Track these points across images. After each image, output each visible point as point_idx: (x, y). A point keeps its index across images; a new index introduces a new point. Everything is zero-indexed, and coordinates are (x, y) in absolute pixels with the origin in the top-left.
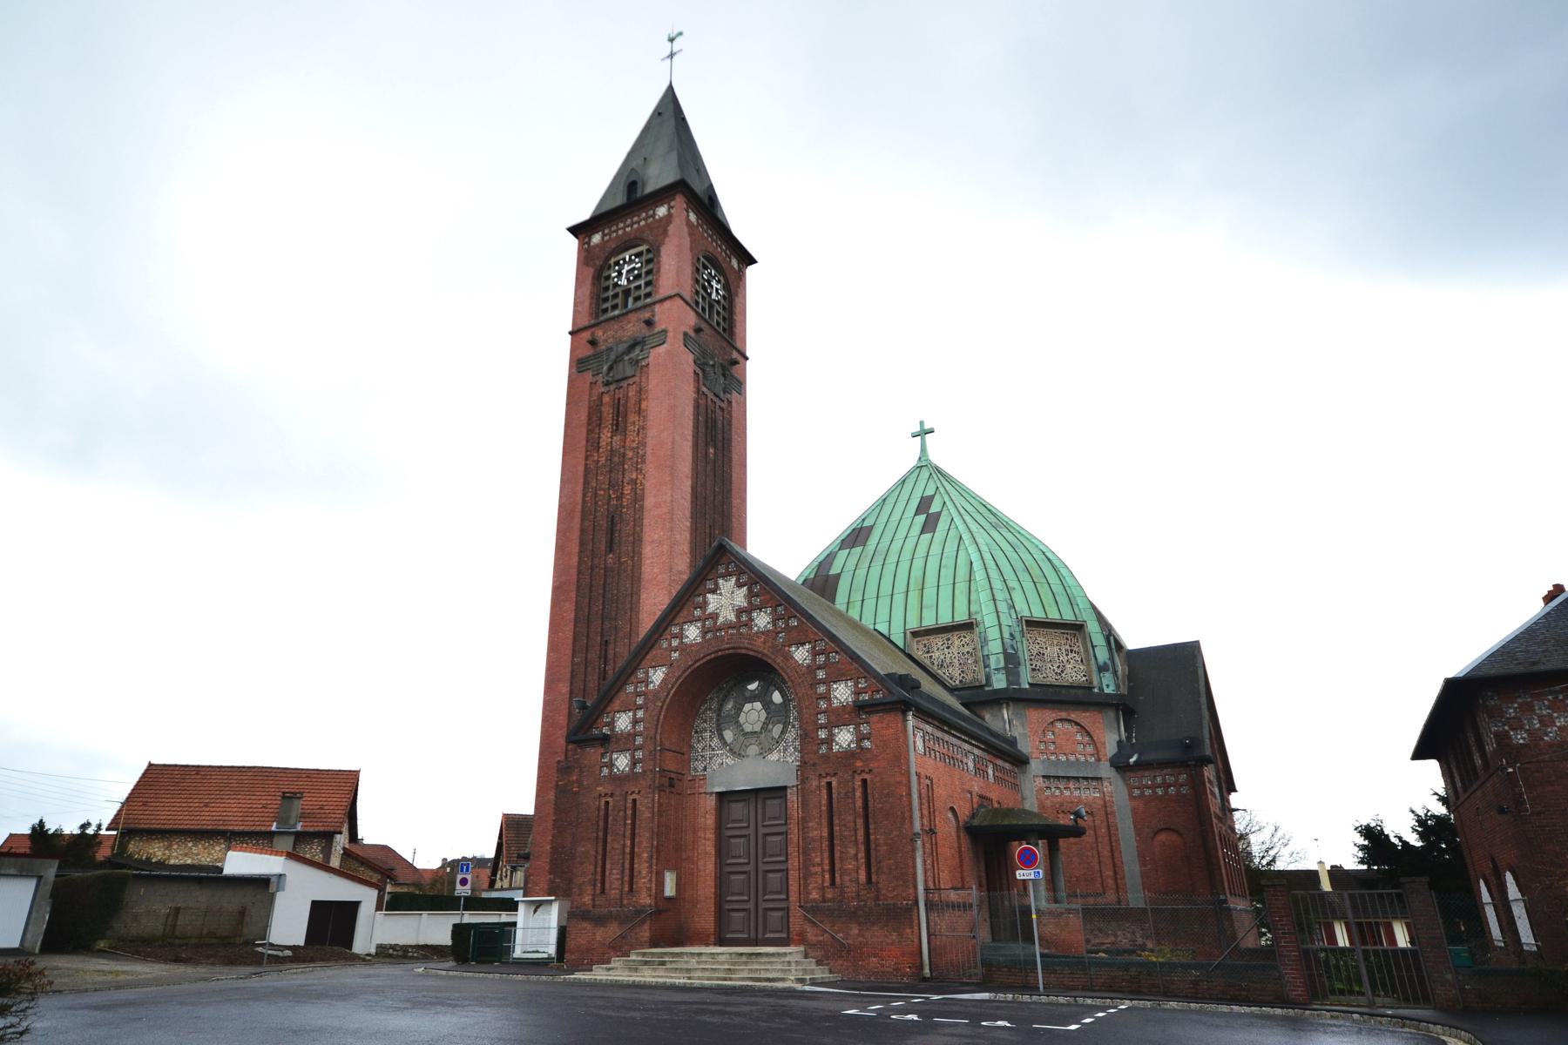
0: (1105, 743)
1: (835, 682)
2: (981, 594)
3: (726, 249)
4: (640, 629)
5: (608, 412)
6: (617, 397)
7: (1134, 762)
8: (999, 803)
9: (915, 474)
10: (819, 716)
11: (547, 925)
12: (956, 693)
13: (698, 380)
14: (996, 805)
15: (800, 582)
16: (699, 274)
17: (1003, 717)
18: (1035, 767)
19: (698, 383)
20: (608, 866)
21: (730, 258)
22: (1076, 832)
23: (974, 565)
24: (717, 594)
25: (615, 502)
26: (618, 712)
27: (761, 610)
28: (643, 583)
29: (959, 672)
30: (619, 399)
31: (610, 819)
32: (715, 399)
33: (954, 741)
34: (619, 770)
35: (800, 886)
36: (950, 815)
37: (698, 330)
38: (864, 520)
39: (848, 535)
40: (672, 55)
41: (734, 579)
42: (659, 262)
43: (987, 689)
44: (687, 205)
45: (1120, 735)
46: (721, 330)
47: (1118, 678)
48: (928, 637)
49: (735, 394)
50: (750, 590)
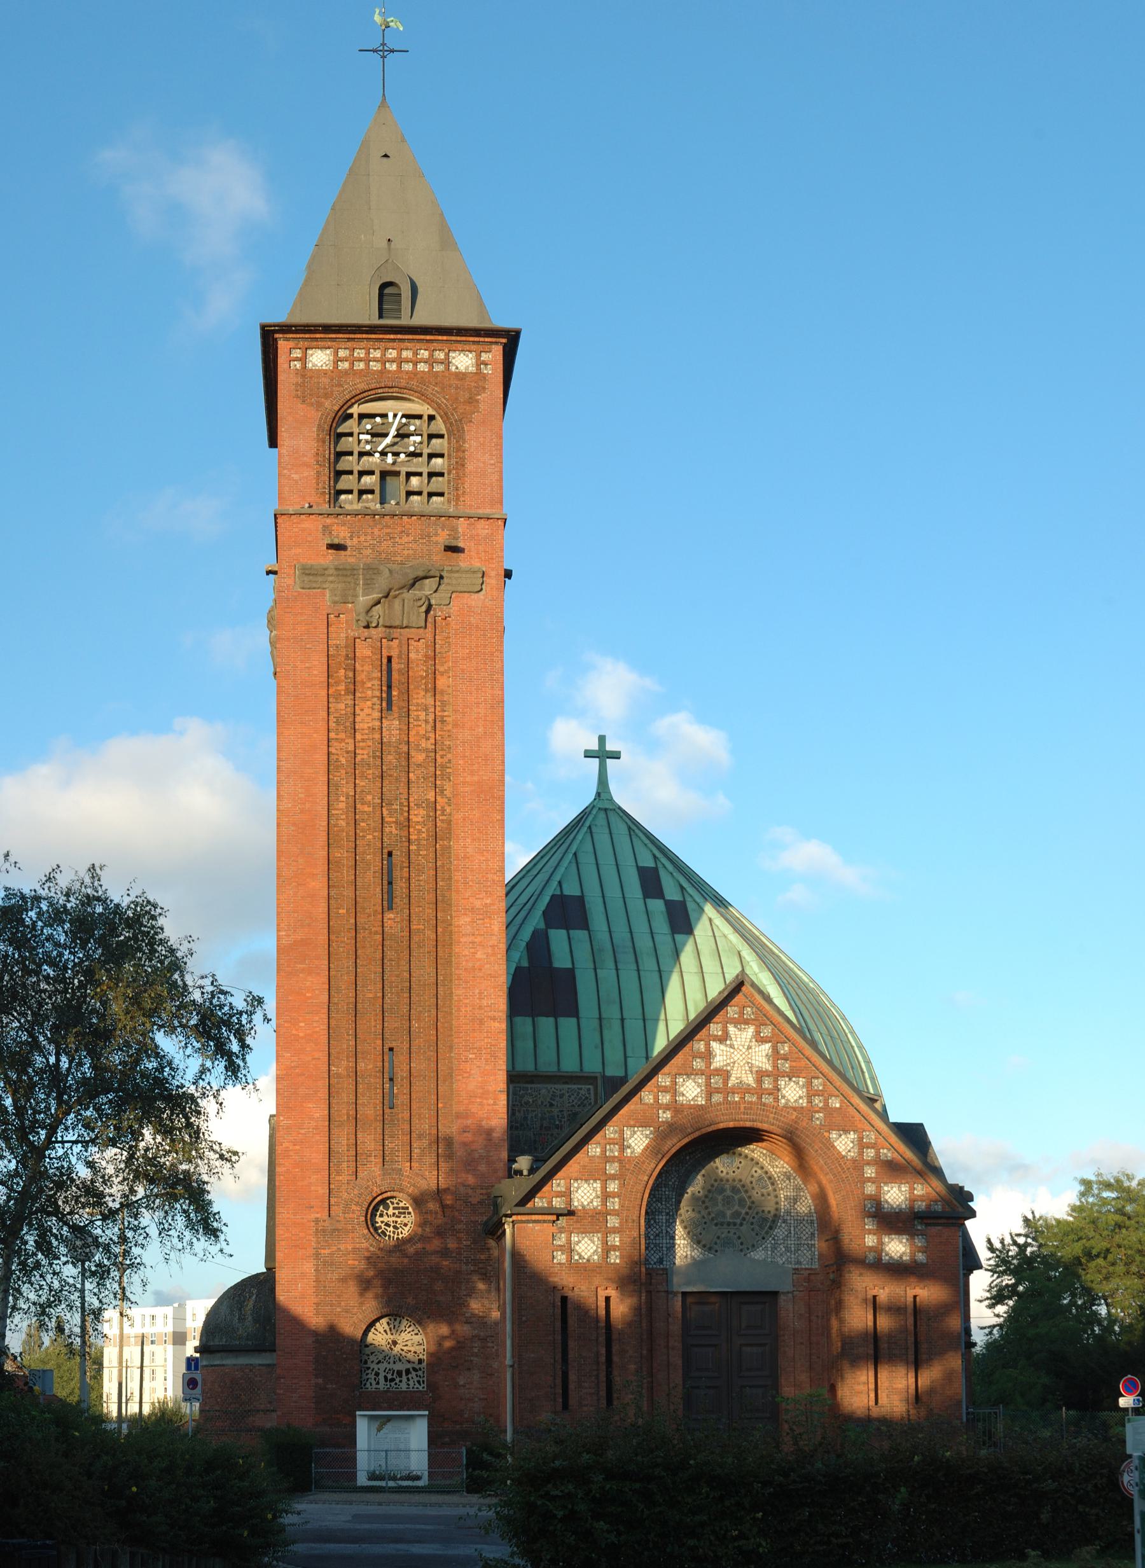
1: (886, 1183)
6: (385, 654)
11: (402, 1447)
24: (726, 1045)
26: (576, 1180)
34: (581, 1257)
41: (751, 1030)
50: (775, 1050)
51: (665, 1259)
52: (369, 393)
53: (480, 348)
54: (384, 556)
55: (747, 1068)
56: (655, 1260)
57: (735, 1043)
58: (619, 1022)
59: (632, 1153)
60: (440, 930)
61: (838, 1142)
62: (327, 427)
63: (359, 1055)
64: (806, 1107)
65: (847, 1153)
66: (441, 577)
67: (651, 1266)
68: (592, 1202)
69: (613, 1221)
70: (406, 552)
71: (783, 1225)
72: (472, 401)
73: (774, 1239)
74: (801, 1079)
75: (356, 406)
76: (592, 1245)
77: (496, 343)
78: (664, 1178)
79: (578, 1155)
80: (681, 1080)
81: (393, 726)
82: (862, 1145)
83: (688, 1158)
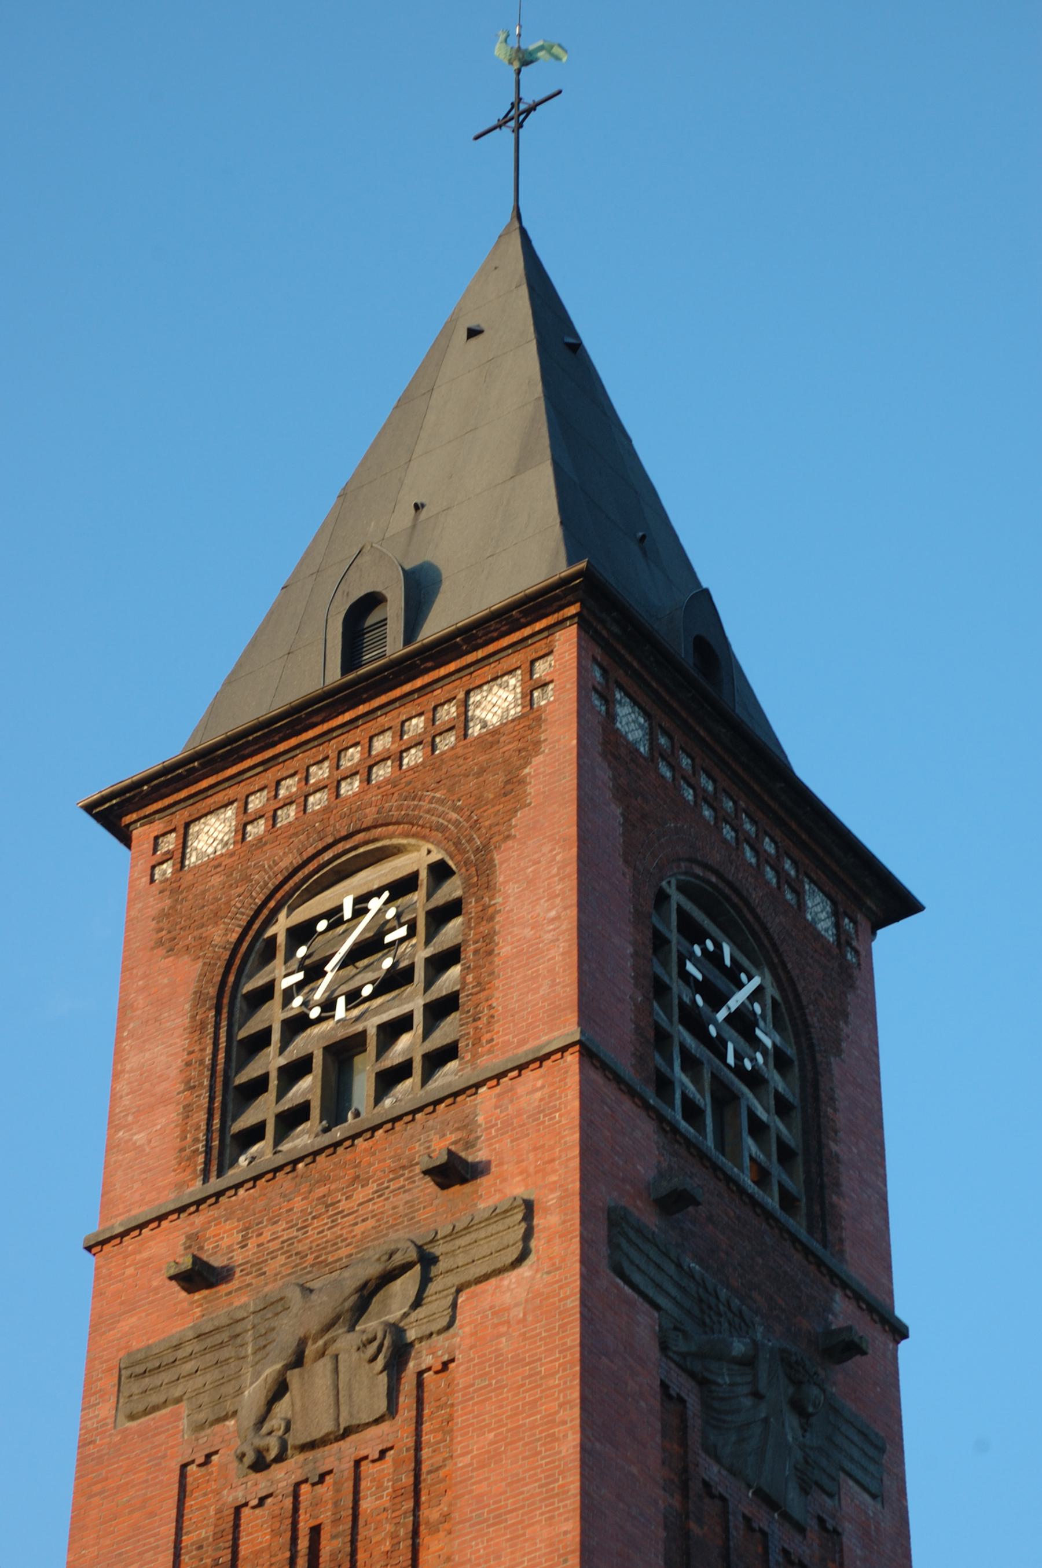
10: (639, 798)
16: (665, 964)
19: (683, 1443)
21: (799, 893)
32: (764, 1519)
42: (487, 915)
44: (605, 672)
46: (772, 1202)
52: (306, 871)
53: (529, 653)
62: (212, 991)
66: (427, 1260)
70: (358, 1230)
75: (282, 916)
77: (560, 624)
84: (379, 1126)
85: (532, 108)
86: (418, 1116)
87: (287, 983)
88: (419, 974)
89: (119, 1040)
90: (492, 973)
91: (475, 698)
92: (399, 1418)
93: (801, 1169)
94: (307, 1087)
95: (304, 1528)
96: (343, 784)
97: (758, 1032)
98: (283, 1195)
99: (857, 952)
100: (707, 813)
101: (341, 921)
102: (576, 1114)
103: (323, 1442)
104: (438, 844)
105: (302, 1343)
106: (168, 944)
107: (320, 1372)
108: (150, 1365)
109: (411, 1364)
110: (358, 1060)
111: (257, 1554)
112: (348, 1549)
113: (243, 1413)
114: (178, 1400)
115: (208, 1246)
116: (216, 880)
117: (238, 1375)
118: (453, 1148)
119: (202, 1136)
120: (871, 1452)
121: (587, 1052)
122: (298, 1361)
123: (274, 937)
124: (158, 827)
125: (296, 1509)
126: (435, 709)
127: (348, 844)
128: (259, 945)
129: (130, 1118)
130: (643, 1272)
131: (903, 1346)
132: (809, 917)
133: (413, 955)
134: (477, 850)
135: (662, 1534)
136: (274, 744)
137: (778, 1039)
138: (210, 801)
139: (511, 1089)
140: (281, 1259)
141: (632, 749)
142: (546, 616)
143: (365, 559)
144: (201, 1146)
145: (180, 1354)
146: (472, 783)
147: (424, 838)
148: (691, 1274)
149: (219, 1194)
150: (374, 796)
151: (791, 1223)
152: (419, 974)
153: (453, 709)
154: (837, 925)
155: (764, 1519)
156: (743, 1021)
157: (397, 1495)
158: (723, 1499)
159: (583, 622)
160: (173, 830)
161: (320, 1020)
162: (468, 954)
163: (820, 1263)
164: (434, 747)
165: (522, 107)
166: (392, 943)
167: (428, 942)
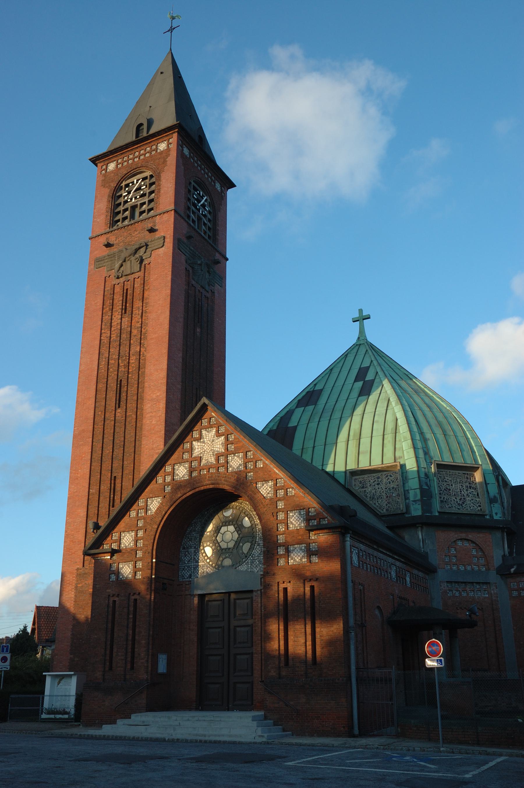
0: (493, 557)
2: (403, 443)
3: (212, 175)
4: (142, 468)
5: (118, 299)
7: (514, 571)
8: (414, 602)
9: (355, 350)
11: (67, 694)
12: (384, 518)
13: (189, 275)
14: (412, 604)
15: (266, 432)
16: (190, 195)
17: (418, 537)
18: (441, 574)
20: (115, 650)
21: (214, 183)
22: (471, 624)
23: (399, 421)
24: (201, 442)
25: (123, 370)
26: (124, 532)
27: (234, 455)
28: (144, 433)
29: (386, 502)
30: (127, 289)
31: (117, 613)
32: (202, 290)
33: (381, 555)
35: (262, 666)
36: (377, 612)
37: (189, 237)
38: (315, 385)
39: (303, 397)
40: (171, 30)
41: (214, 430)
42: (159, 185)
43: (407, 516)
45: (504, 552)
46: (207, 238)
47: (504, 508)
48: (363, 476)
49: (217, 287)
50: (227, 439)
51: (192, 575)
53: (168, 137)
54: (127, 244)
55: (211, 453)
56: (187, 576)
57: (205, 440)
58: (312, 449)
59: (151, 513)
60: (138, 413)
61: (262, 489)
62: (111, 195)
63: (102, 482)
64: (243, 470)
65: (267, 495)
66: (147, 245)
67: (185, 580)
68: (130, 544)
69: (140, 554)
71: (258, 547)
72: (165, 162)
73: (252, 557)
74: (240, 454)
76: (129, 569)
77: (174, 132)
78: (193, 527)
79: (124, 518)
80: (177, 467)
81: (126, 320)
82: (276, 489)
83: (206, 513)
84: (139, 221)
85: (174, 28)
86: (146, 220)
87: (124, 194)
88: (147, 195)
89: (95, 202)
90: (160, 196)
91: (159, 145)
92: (141, 272)
93: (212, 231)
94: (127, 213)
95: (119, 380)
96: (135, 159)
97: (206, 208)
98: (123, 232)
99: (224, 194)
100: (199, 168)
101: (134, 184)
102: (173, 222)
103: (129, 275)
104: (151, 171)
105: (125, 258)
106: (104, 186)
107: (128, 263)
108: (100, 260)
109: (144, 263)
110: (136, 209)
111: (118, 292)
112: (132, 293)
113: (115, 269)
114: (105, 266)
115: (110, 240)
116: (112, 175)
117: (115, 262)
118: (152, 226)
119: (109, 221)
120: (221, 279)
121: (175, 211)
122: (125, 261)
123: (122, 186)
124: (102, 164)
125: (124, 285)
126: (152, 146)
127: (136, 170)
128: (119, 187)
129: (97, 217)
130: (183, 249)
131: (227, 261)
132: (216, 187)
133: (146, 191)
134: (158, 173)
135: (184, 293)
136: (123, 150)
137: (209, 209)
138: (111, 160)
139: (162, 217)
140: (122, 243)
141: (186, 157)
142: (171, 131)
143: (140, 116)
144: (109, 223)
145: (105, 258)
146: (158, 161)
147: (149, 170)
148: (192, 250)
149: (112, 231)
150: (140, 162)
151: (209, 241)
152: (147, 195)
153: (155, 147)
154: (221, 189)
155: (202, 290)
156: (203, 206)
157: (141, 284)
158: (195, 287)
159: (178, 132)
160: (105, 165)
161: (130, 201)
162: (156, 192)
163: (214, 248)
164: (151, 153)
165: (172, 28)
166: (143, 189)
167: (149, 189)
